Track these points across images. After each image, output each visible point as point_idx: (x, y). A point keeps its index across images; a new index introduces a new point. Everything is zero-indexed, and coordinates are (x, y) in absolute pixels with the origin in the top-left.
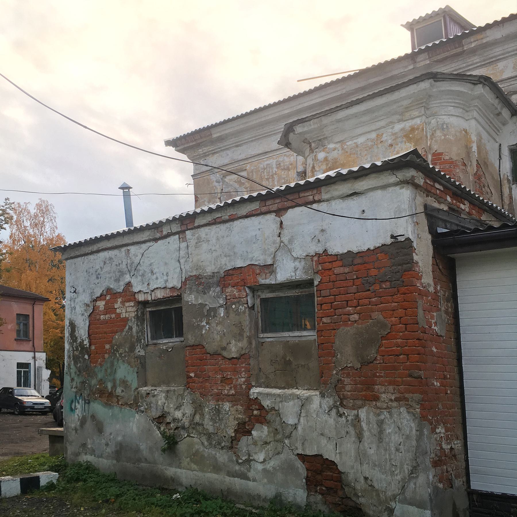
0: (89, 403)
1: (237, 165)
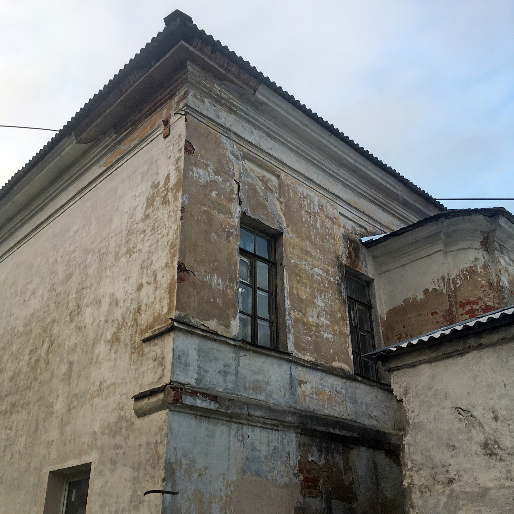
1: (266, 159)
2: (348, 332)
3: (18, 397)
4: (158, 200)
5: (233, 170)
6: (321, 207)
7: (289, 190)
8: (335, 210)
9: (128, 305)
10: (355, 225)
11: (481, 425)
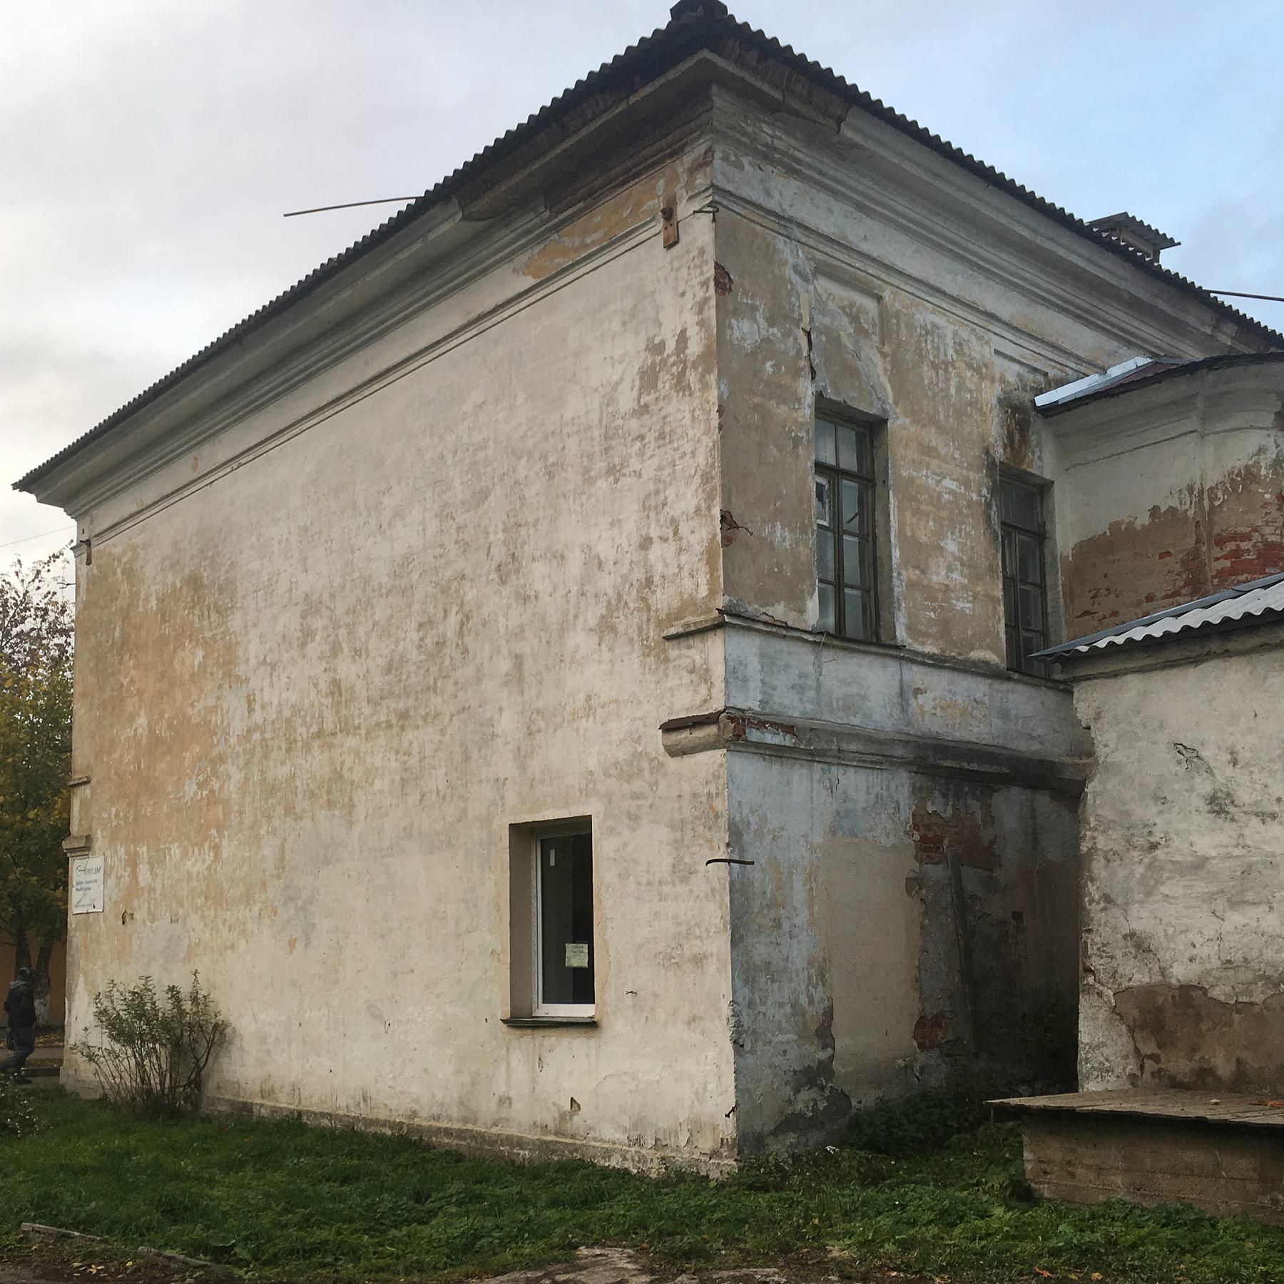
2: (999, 594)
3: (411, 702)
4: (665, 382)
5: (799, 307)
6: (959, 346)
7: (898, 324)
8: (986, 348)
9: (625, 570)
11: (1210, 771)
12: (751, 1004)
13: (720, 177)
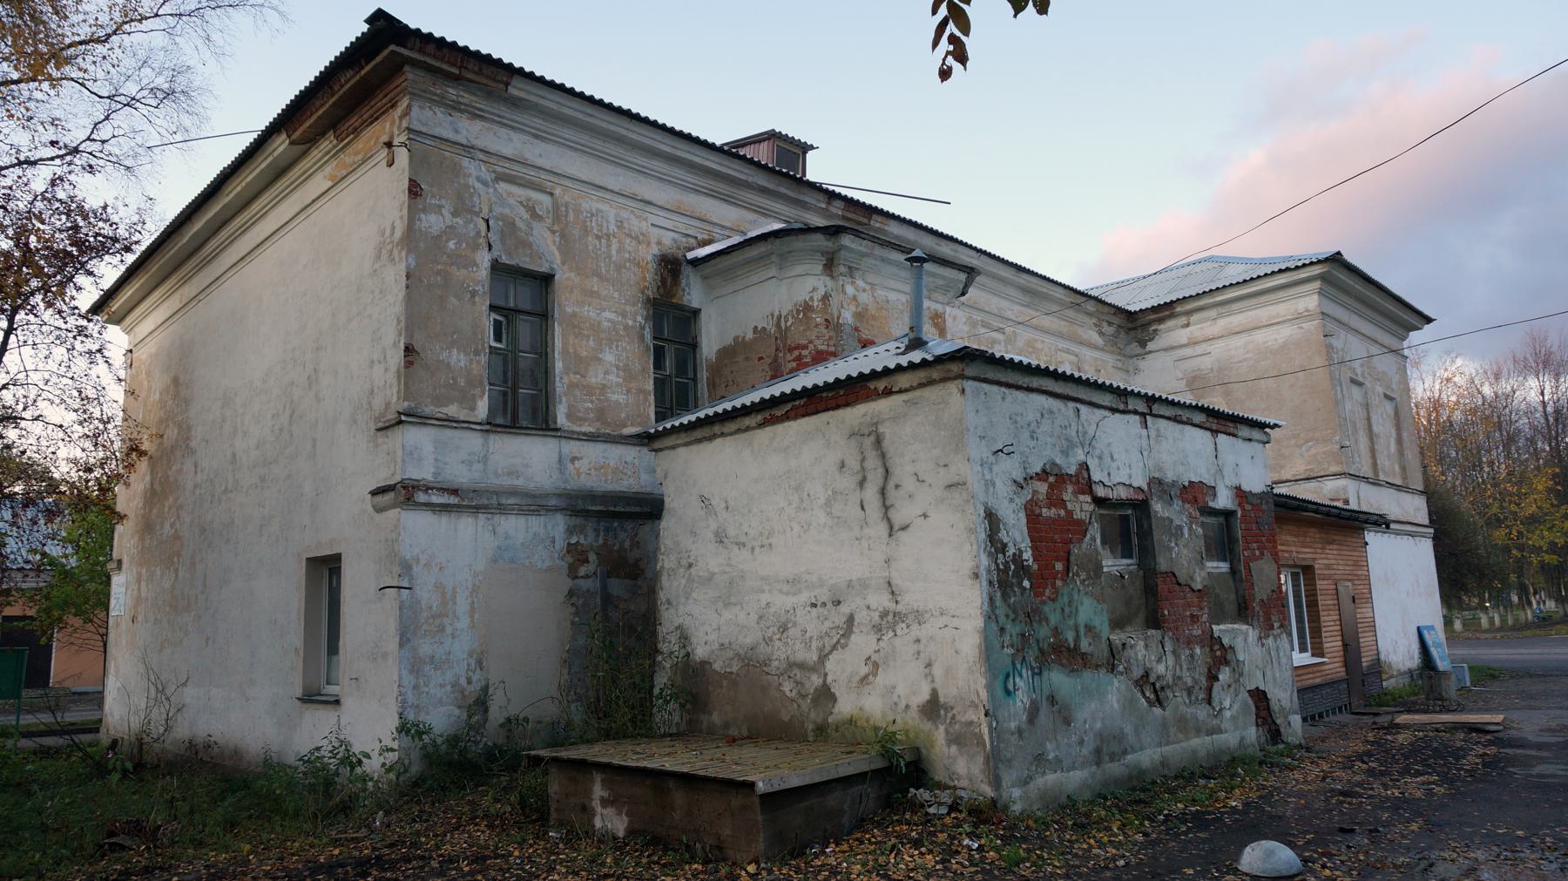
0: (1040, 674)
7: (567, 211)
10: (676, 236)
12: (416, 687)
13: (415, 122)
